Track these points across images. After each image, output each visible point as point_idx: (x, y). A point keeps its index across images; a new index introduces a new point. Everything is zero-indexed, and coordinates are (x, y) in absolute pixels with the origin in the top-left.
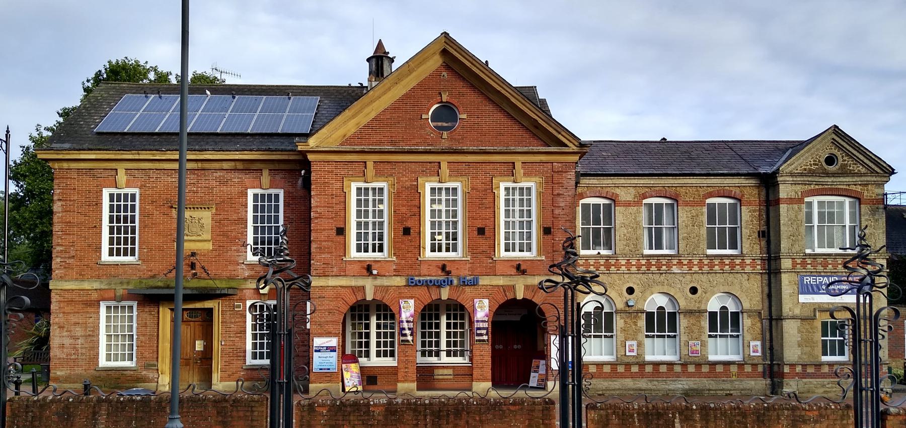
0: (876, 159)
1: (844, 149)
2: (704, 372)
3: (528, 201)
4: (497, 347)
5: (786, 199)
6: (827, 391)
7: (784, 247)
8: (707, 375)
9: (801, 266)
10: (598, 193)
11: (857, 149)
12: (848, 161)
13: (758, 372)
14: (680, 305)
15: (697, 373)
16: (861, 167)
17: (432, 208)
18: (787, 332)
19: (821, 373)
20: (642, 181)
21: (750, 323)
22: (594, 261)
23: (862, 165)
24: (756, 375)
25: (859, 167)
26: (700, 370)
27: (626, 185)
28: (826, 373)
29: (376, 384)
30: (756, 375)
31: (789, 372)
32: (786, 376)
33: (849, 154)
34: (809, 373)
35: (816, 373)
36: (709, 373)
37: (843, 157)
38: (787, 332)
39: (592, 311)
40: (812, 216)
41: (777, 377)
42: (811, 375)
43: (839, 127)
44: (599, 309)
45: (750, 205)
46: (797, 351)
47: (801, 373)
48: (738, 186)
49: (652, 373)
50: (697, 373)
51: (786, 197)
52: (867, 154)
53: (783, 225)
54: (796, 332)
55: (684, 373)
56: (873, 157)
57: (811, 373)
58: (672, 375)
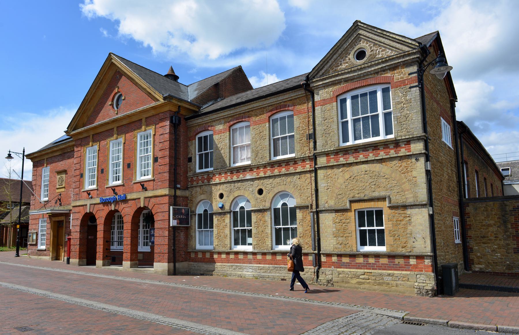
0: (400, 38)
1: (370, 40)
2: (269, 260)
3: (357, 135)
4: (93, 237)
5: (320, 101)
6: (360, 282)
7: (319, 145)
8: (270, 262)
9: (334, 160)
10: (203, 128)
11: (382, 35)
12: (376, 50)
13: (309, 261)
14: (229, 205)
15: (263, 260)
16: (390, 51)
17: (315, 152)
18: (323, 223)
19: (357, 263)
20: (226, 113)
21: (302, 216)
22: (201, 177)
23: (389, 49)
24: (308, 263)
25: (388, 52)
26: (265, 258)
27: (218, 119)
28: (360, 263)
29: (115, 262)
30: (308, 263)
31: (325, 261)
32: (324, 265)
33: (376, 42)
34: (344, 263)
35: (351, 263)
36: (272, 260)
37: (371, 48)
38: (323, 223)
39: (203, 213)
40: (352, 112)
41: (471, 273)
42: (346, 265)
43: (362, 21)
44: (206, 211)
45: (300, 114)
46: (332, 241)
47: (336, 263)
48: (291, 100)
49: (234, 259)
50: (263, 260)
51: (320, 99)
52: (391, 37)
53: (318, 125)
54: (331, 223)
55: (254, 260)
56: (397, 37)
57: (346, 263)
58: (246, 261)
